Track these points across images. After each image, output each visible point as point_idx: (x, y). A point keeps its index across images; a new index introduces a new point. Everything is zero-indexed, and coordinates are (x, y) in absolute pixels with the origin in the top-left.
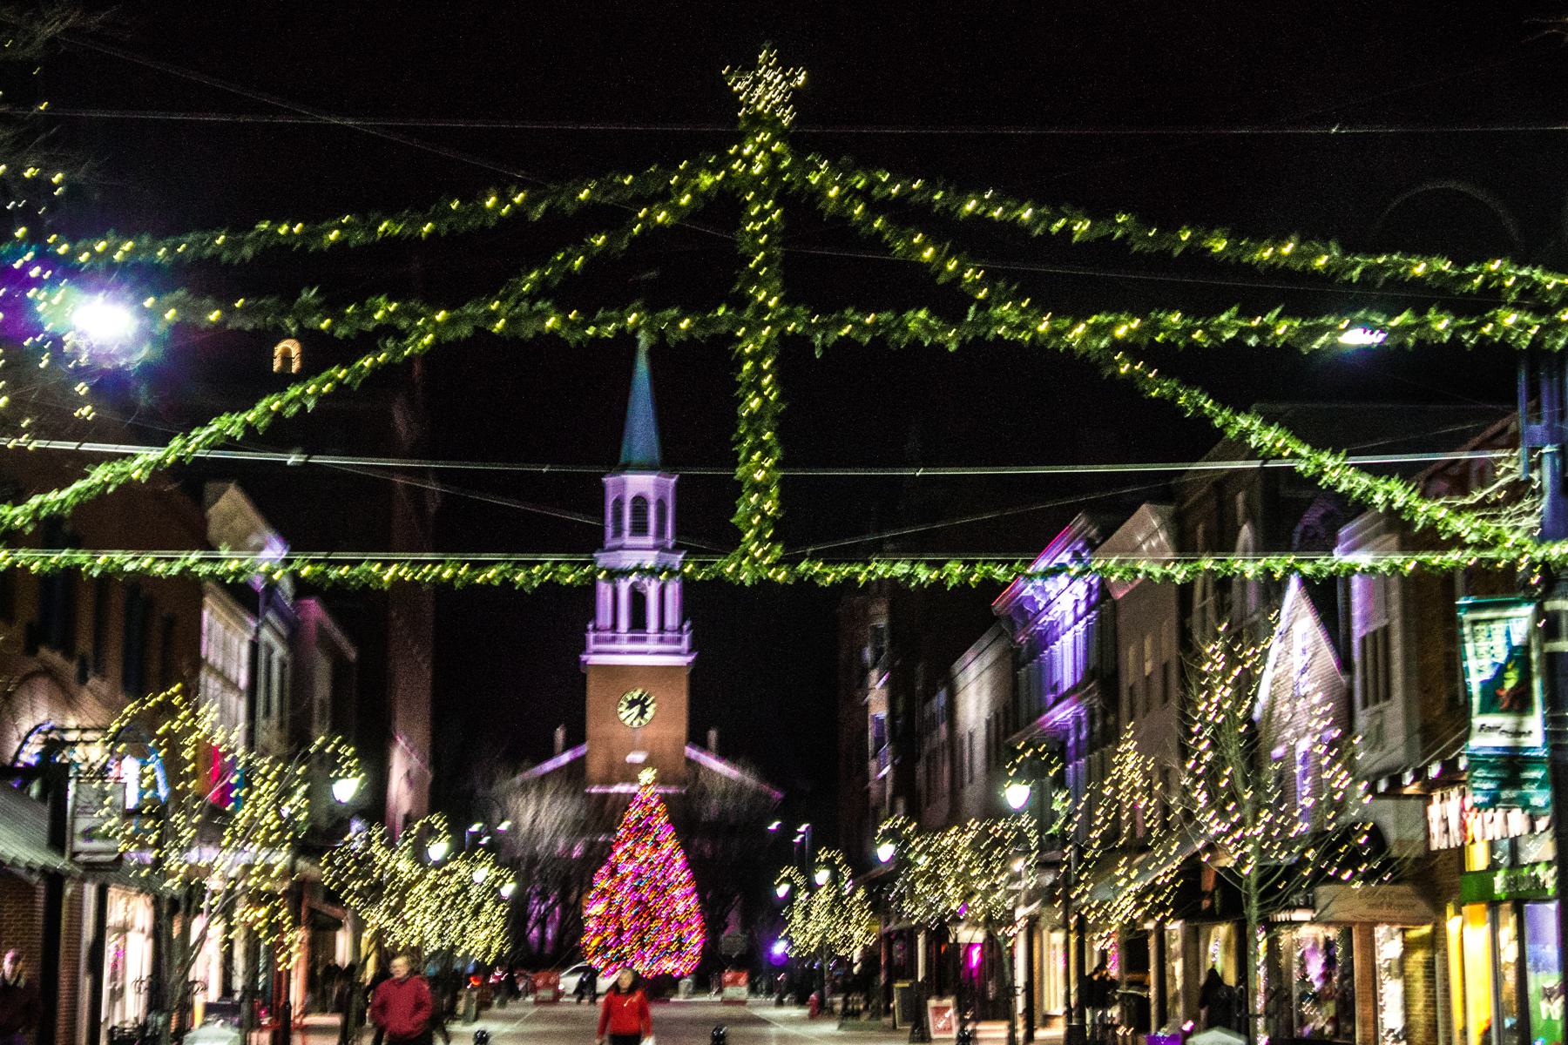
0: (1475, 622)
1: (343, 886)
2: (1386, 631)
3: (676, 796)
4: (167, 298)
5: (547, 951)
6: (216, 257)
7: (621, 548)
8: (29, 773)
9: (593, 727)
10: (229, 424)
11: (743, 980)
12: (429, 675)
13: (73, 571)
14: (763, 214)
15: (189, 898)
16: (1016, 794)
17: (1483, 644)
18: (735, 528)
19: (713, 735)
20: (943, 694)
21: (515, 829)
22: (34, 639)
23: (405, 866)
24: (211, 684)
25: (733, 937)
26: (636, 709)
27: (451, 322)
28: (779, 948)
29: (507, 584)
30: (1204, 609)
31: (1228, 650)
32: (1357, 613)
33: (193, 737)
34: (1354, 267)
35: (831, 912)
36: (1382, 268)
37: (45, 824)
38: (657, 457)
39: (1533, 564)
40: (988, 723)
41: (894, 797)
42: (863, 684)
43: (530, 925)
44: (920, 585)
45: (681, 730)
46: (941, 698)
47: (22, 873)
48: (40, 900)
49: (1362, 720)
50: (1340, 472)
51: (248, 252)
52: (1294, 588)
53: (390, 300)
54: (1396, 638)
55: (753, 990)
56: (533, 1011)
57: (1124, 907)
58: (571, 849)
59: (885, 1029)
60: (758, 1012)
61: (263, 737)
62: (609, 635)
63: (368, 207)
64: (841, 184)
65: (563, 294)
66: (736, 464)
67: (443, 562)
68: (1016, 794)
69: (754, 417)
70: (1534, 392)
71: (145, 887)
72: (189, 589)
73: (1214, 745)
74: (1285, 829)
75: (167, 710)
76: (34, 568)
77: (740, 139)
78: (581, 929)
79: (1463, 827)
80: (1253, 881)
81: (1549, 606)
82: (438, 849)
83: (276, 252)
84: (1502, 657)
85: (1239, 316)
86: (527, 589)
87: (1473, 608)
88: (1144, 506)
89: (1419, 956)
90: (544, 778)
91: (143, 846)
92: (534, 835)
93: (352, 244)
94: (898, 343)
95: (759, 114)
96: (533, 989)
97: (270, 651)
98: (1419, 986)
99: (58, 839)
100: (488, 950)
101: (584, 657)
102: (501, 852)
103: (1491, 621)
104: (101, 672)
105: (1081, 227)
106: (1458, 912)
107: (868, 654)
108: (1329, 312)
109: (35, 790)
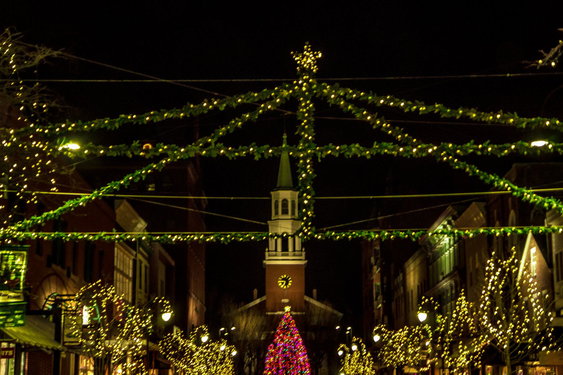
1: (167, 353)
3: (302, 316)
6: (106, 128)
7: (278, 219)
8: (48, 313)
9: (268, 290)
10: (114, 185)
12: (204, 270)
13: (59, 239)
14: (307, 105)
16: (422, 317)
19: (315, 291)
20: (401, 275)
21: (238, 329)
22: (50, 261)
24: (118, 276)
27: (186, 152)
31: (496, 262)
32: (554, 245)
33: (106, 299)
34: (523, 122)
35: (359, 361)
36: (534, 122)
37: (54, 330)
38: (291, 185)
40: (418, 286)
41: (383, 316)
43: (245, 365)
44: (372, 240)
45: (303, 290)
46: (401, 277)
47: (45, 350)
50: (529, 195)
51: (117, 125)
52: (530, 235)
53: (165, 145)
57: (463, 360)
58: (260, 337)
62: (274, 253)
63: (159, 107)
64: (335, 94)
65: (226, 140)
67: (194, 234)
69: (304, 180)
71: (89, 355)
74: (520, 330)
76: (46, 238)
77: (298, 78)
83: (127, 125)
85: (474, 144)
86: (226, 243)
88: (474, 203)
90: (249, 309)
91: (88, 339)
92: (245, 332)
93: (155, 121)
94: (348, 156)
97: (141, 262)
99: (58, 337)
104: (76, 274)
107: (373, 260)
108: (507, 142)
109: (51, 318)
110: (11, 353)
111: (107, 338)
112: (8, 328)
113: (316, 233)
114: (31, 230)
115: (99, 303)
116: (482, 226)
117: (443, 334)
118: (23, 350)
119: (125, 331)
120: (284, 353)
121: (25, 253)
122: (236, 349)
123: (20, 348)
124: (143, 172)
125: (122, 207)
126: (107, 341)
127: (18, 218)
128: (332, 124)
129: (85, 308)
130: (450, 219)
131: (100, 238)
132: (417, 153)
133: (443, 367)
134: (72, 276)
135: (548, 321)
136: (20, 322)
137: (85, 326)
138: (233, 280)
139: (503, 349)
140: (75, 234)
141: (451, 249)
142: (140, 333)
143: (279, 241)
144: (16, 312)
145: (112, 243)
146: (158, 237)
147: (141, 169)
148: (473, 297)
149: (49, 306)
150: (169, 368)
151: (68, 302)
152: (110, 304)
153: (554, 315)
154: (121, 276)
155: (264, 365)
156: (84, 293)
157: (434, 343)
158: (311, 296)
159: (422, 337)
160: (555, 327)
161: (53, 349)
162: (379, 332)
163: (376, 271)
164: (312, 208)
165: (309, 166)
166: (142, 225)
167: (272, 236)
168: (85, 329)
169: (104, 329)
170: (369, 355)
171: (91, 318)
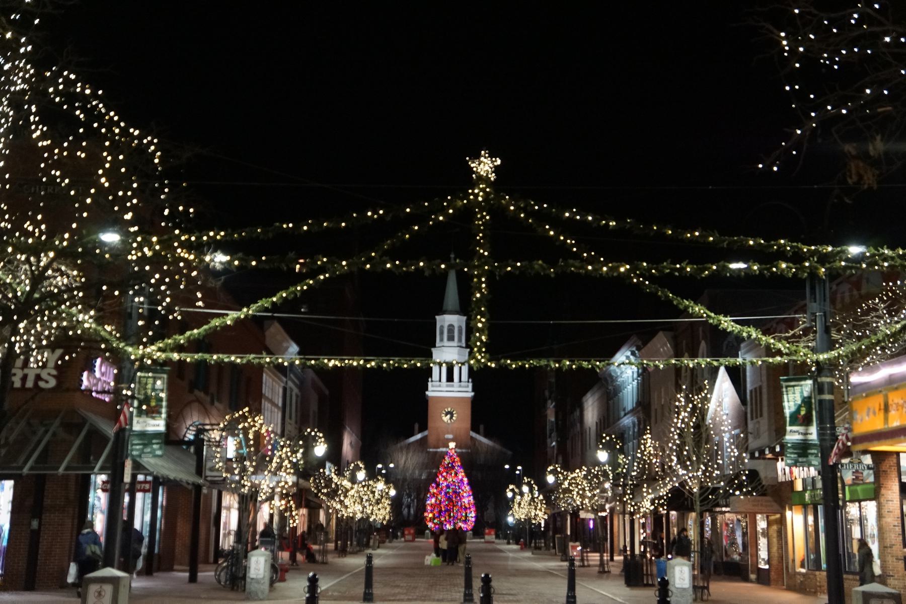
2: (760, 387)
5: (411, 518)
8: (190, 443)
10: (265, 303)
11: (493, 533)
13: (203, 362)
16: (603, 456)
17: (791, 396)
19: (482, 427)
21: (396, 467)
22: (193, 387)
23: (346, 484)
24: (266, 405)
25: (490, 513)
26: (449, 416)
29: (380, 367)
32: (748, 379)
34: (724, 241)
35: (530, 504)
37: (195, 463)
42: (545, 407)
45: (467, 424)
46: (578, 413)
47: (185, 485)
50: (727, 323)
51: (270, 235)
52: (722, 370)
54: (765, 390)
55: (497, 537)
56: (402, 545)
57: (647, 505)
58: (421, 475)
59: (551, 555)
60: (499, 547)
61: (288, 428)
62: (438, 383)
70: (813, 289)
71: (233, 491)
74: (711, 473)
75: (244, 418)
78: (425, 510)
79: (791, 473)
80: (697, 495)
81: (819, 380)
84: (799, 402)
87: (786, 381)
89: (775, 527)
90: (409, 444)
96: (403, 535)
97: (291, 390)
98: (775, 540)
99: (199, 471)
100: (384, 519)
101: (427, 393)
102: (389, 479)
103: (793, 386)
104: (220, 401)
106: (791, 509)
107: (547, 393)
108: (708, 262)
109: (192, 449)
110: (147, 486)
111: (253, 473)
112: (145, 459)
113: (489, 361)
114: (172, 350)
115: (246, 434)
116: (671, 357)
117: (625, 476)
118: (161, 484)
119: (274, 465)
120: (446, 493)
121: (165, 376)
122: (395, 488)
123: (157, 482)
124: (299, 288)
126: (254, 477)
127: (159, 336)
128: (508, 237)
129: (230, 439)
130: (634, 349)
131: (249, 361)
133: (624, 513)
134: (216, 404)
135: (743, 463)
136: (159, 453)
137: (231, 460)
138: (388, 413)
139: (692, 494)
140: (221, 356)
141: (635, 383)
142: (291, 468)
144: (154, 441)
145: (261, 367)
146: (313, 362)
147: (296, 285)
148: (661, 437)
149: (190, 436)
150: (321, 507)
151: (211, 432)
152: (257, 434)
153: (748, 457)
154: (269, 405)
155: (424, 506)
156: (229, 422)
157: (615, 485)
158: (478, 432)
159: (602, 479)
160: (749, 471)
161: (193, 484)
162: (555, 472)
163: (551, 407)
164: (486, 332)
165: (484, 285)
166: (294, 348)
168: (229, 463)
169: (251, 463)
170: (541, 497)
171: (237, 450)
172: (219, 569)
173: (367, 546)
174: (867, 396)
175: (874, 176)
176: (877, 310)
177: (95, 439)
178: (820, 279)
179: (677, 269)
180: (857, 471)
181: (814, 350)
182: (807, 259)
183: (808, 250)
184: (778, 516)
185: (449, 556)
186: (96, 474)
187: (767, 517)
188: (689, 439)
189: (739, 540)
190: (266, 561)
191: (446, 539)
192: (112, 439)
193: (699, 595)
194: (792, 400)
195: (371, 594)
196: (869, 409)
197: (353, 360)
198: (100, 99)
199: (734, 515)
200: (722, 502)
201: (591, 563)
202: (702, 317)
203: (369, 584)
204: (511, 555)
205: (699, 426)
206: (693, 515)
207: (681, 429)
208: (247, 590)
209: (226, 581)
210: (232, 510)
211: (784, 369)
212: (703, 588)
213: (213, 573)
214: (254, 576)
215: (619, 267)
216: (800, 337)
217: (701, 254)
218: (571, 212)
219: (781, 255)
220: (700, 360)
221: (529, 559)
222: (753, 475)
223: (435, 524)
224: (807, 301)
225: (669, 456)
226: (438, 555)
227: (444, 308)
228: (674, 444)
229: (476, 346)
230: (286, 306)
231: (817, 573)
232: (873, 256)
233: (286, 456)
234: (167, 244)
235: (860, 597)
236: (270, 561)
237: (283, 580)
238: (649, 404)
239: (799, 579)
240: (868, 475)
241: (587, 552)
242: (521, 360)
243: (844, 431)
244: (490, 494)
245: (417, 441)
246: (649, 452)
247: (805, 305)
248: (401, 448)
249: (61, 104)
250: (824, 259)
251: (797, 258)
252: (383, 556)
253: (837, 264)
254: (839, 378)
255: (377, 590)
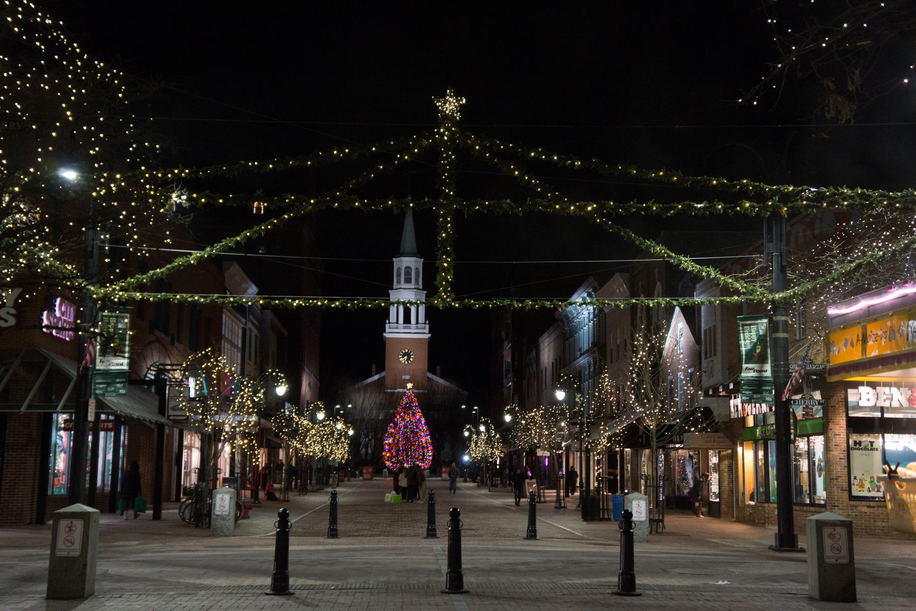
0: (743, 325)
2: (715, 327)
4: (202, 194)
10: (229, 242)
13: (167, 301)
15: (215, 435)
17: (747, 335)
18: (436, 286)
19: (438, 368)
21: (354, 407)
24: (226, 345)
25: (446, 452)
28: (466, 458)
29: (344, 307)
30: (641, 317)
36: (94, 348)
37: (157, 403)
38: (415, 251)
39: (768, 301)
45: (426, 366)
46: (534, 353)
47: (148, 423)
48: (156, 434)
49: (704, 364)
50: (687, 263)
54: (719, 331)
61: (247, 368)
62: (395, 325)
66: (437, 259)
68: (560, 395)
70: (770, 230)
71: (198, 431)
72: (216, 310)
73: (638, 375)
74: (668, 410)
75: (207, 358)
78: (383, 450)
79: (743, 409)
80: (654, 432)
82: (321, 416)
84: (755, 340)
85: (638, 202)
87: (742, 319)
89: (726, 462)
90: (367, 385)
91: (196, 413)
95: (447, 115)
96: (361, 474)
97: (251, 332)
99: (162, 410)
100: (343, 458)
102: (348, 420)
103: (750, 325)
105: (578, 163)
106: (742, 445)
107: (503, 334)
113: (454, 300)
114: (135, 290)
123: (120, 420)
125: (231, 270)
127: (123, 276)
132: (574, 211)
134: (176, 344)
136: (122, 391)
137: (193, 399)
138: (347, 354)
140: (184, 295)
143: (401, 309)
144: (118, 380)
147: (260, 224)
149: (151, 376)
157: (572, 424)
158: (435, 373)
162: (511, 412)
166: (253, 289)
167: (393, 304)
172: (183, 507)
173: (327, 484)
174: (844, 328)
175: (851, 111)
176: (832, 250)
177: (57, 380)
178: (781, 216)
179: (643, 208)
180: (807, 407)
181: (771, 290)
182: (771, 198)
183: (770, 190)
184: (730, 451)
185: (409, 493)
186: (58, 413)
187: (719, 452)
188: (647, 378)
189: (690, 476)
190: (231, 498)
191: (406, 476)
192: (75, 378)
193: (654, 527)
194: (747, 339)
195: (336, 530)
196: (846, 340)
197: (317, 299)
198: (63, 30)
199: (687, 451)
200: (675, 438)
201: (547, 499)
202: (201, 382)
203: (333, 520)
204: (468, 492)
205: (655, 365)
206: (647, 451)
207: (640, 368)
208: (212, 526)
209: (191, 518)
210: (193, 449)
211: (739, 307)
212: (658, 521)
213: (177, 511)
214: (220, 513)
215: (586, 206)
216: (756, 276)
217: (666, 193)
218: (536, 152)
219: (744, 194)
220: (660, 299)
221: (487, 496)
222: (707, 412)
223: (393, 463)
224: (765, 240)
225: (627, 394)
226: (397, 493)
227: (401, 251)
228: (632, 382)
229: (442, 285)
230: (250, 245)
231: (766, 505)
232: (833, 195)
233: (246, 396)
234: (132, 181)
235: (814, 525)
236: (234, 500)
237: (246, 517)
238: (605, 344)
239: (749, 511)
240: (817, 410)
241: (544, 489)
242: (484, 300)
243: (797, 368)
244: (447, 431)
245: (374, 382)
246: (606, 391)
247: (762, 244)
248: (359, 389)
249: (20, 34)
250: (786, 198)
251: (759, 197)
252: (346, 494)
253: (799, 203)
254: (792, 317)
255: (341, 527)
